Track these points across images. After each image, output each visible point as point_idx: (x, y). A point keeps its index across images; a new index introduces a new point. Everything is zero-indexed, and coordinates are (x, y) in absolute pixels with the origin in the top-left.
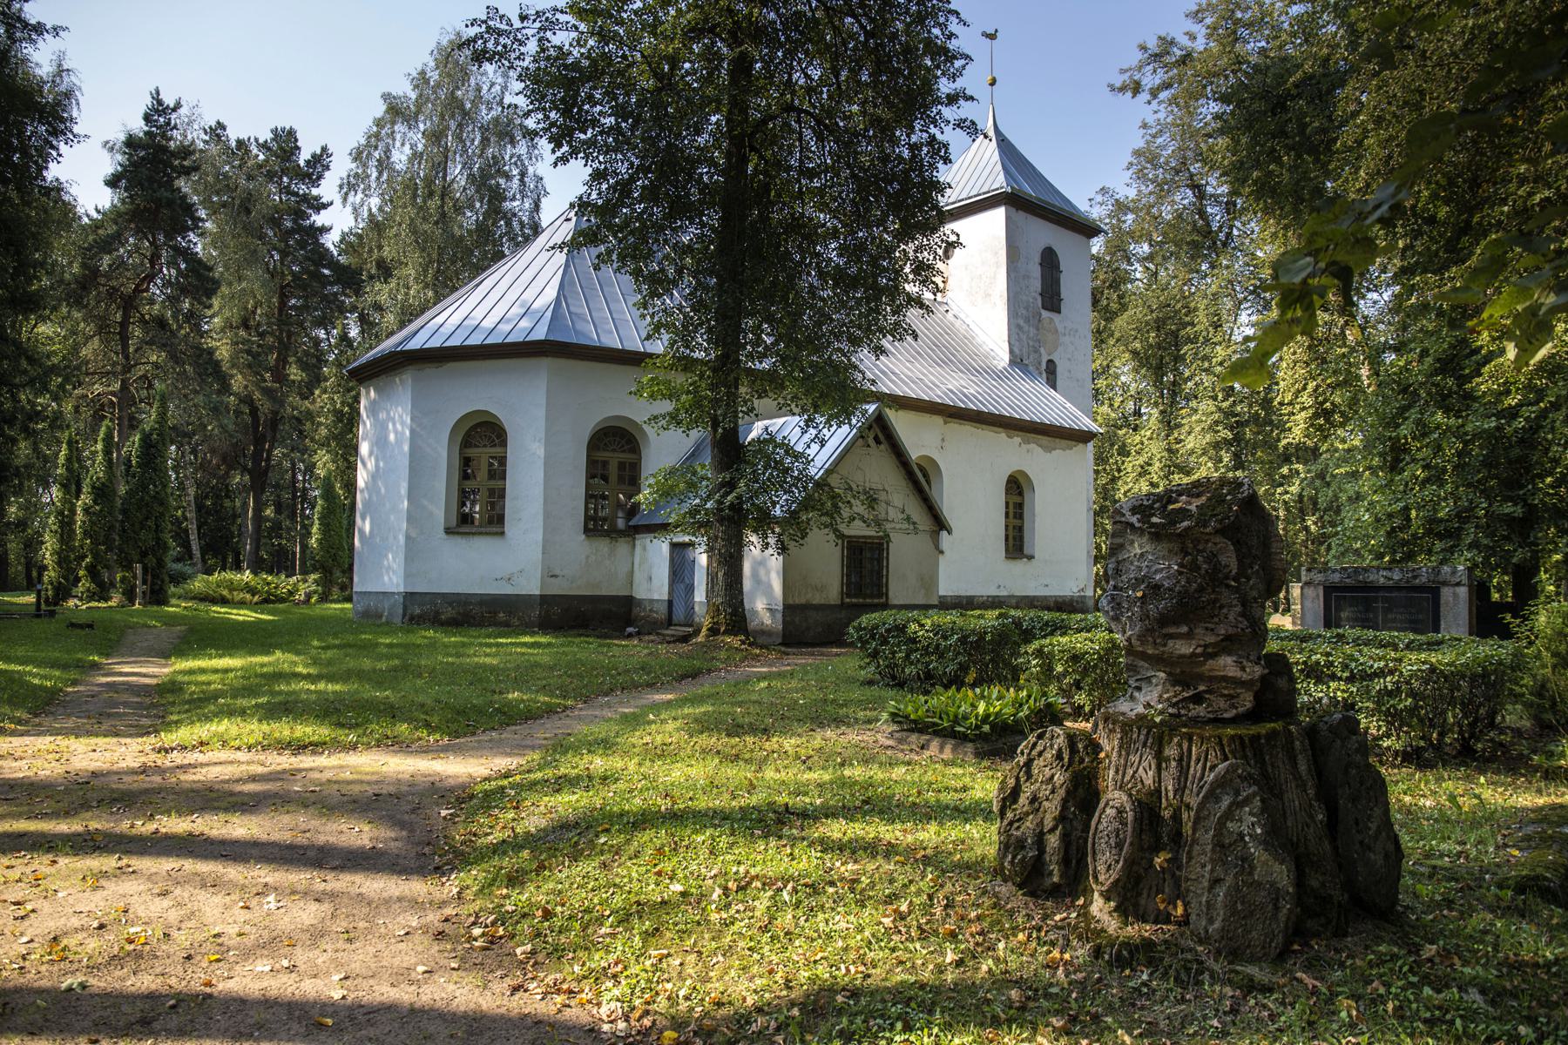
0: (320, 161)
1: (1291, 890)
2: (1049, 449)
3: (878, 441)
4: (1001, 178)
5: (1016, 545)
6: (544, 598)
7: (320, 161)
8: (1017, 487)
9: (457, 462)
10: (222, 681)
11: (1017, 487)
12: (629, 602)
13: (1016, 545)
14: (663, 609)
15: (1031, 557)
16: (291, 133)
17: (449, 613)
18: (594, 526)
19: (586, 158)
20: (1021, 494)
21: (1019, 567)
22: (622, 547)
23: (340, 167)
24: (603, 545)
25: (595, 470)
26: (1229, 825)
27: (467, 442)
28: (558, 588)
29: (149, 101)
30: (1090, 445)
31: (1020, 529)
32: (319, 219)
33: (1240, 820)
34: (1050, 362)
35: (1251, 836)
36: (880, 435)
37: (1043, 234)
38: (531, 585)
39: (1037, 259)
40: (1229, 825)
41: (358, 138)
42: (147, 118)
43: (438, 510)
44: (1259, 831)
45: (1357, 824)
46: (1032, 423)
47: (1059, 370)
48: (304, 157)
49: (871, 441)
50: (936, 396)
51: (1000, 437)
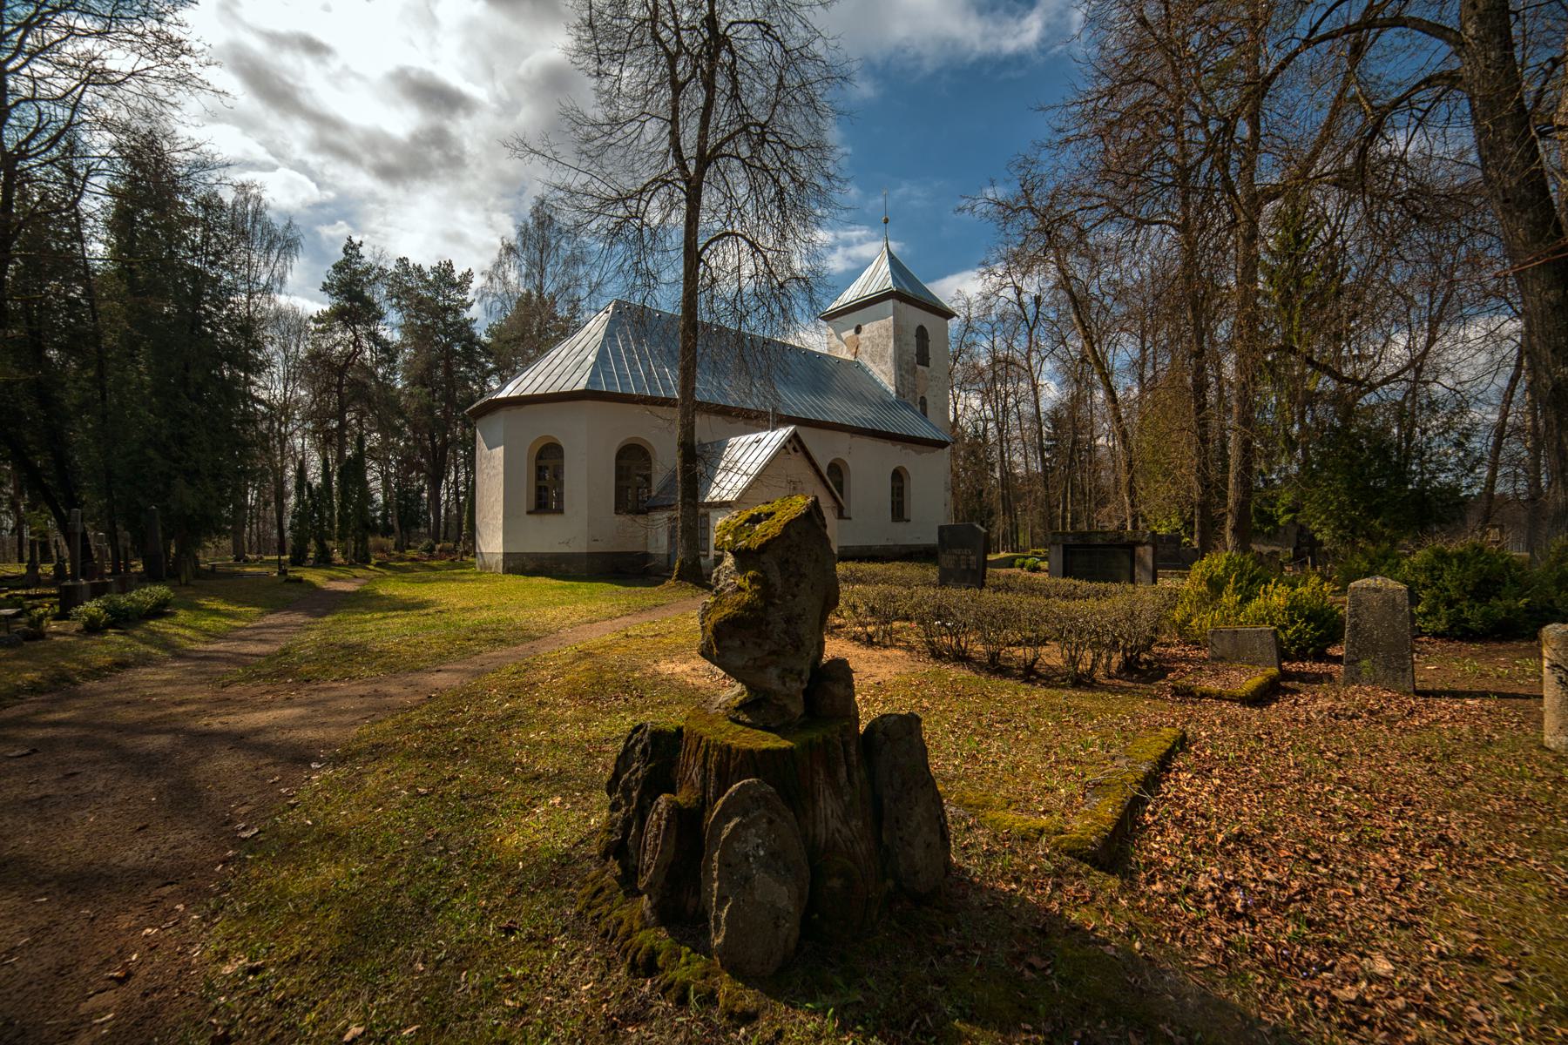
0: (467, 276)
1: (791, 909)
2: (919, 453)
3: (795, 450)
4: (890, 281)
5: (899, 512)
6: (590, 555)
7: (467, 276)
8: (898, 476)
9: (533, 468)
10: (1058, 516)
11: (898, 476)
12: (646, 556)
13: (899, 512)
14: (665, 561)
15: (908, 521)
16: (450, 264)
17: (530, 566)
18: (621, 506)
19: (1401, 476)
20: (902, 481)
21: (900, 526)
22: (641, 520)
23: (478, 282)
24: (624, 519)
25: (622, 474)
26: (736, 845)
27: (540, 456)
28: (600, 547)
29: (346, 242)
30: (948, 449)
31: (902, 502)
32: (467, 315)
33: (746, 841)
34: (922, 398)
35: (754, 857)
36: (798, 448)
37: (918, 317)
38: (580, 546)
39: (914, 332)
40: (736, 845)
41: (488, 267)
42: (345, 251)
43: (525, 497)
44: (762, 853)
45: (898, 822)
46: (922, 438)
47: (929, 402)
48: (457, 275)
49: (791, 451)
50: (846, 421)
51: (887, 446)
